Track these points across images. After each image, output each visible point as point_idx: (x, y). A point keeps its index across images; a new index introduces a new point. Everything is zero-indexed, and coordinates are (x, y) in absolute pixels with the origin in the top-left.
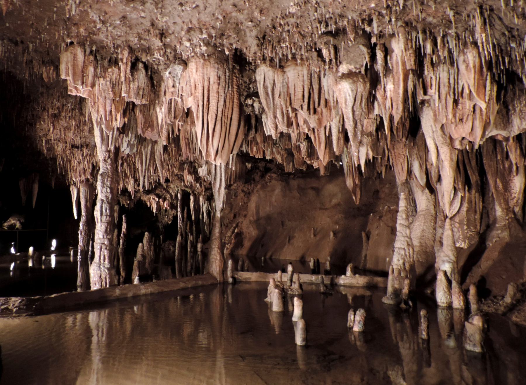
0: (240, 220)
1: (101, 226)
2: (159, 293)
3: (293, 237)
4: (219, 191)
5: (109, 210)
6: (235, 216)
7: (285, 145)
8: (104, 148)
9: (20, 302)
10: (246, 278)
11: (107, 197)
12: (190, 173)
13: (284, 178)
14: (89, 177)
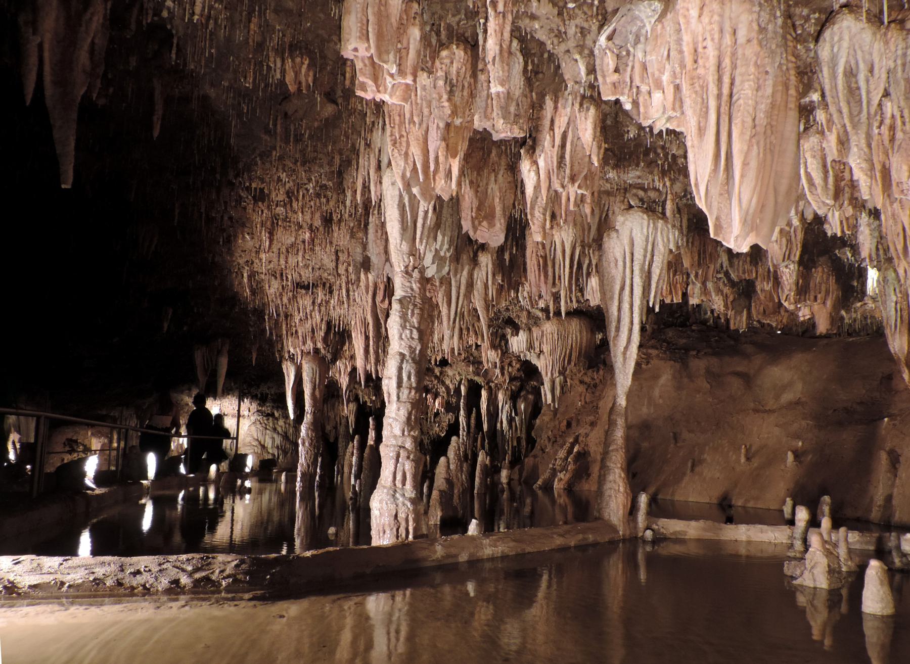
0: (582, 431)
1: (399, 409)
2: (517, 555)
3: (701, 462)
4: (624, 353)
5: (416, 375)
6: (569, 425)
7: (744, 273)
8: (405, 247)
9: (237, 566)
10: (675, 533)
11: (412, 350)
12: (494, 347)
13: (677, 355)
14: (320, 345)
